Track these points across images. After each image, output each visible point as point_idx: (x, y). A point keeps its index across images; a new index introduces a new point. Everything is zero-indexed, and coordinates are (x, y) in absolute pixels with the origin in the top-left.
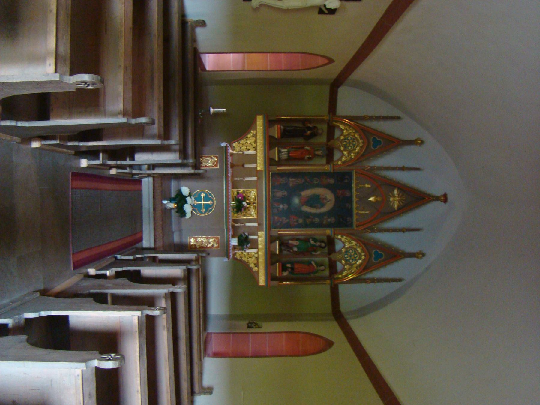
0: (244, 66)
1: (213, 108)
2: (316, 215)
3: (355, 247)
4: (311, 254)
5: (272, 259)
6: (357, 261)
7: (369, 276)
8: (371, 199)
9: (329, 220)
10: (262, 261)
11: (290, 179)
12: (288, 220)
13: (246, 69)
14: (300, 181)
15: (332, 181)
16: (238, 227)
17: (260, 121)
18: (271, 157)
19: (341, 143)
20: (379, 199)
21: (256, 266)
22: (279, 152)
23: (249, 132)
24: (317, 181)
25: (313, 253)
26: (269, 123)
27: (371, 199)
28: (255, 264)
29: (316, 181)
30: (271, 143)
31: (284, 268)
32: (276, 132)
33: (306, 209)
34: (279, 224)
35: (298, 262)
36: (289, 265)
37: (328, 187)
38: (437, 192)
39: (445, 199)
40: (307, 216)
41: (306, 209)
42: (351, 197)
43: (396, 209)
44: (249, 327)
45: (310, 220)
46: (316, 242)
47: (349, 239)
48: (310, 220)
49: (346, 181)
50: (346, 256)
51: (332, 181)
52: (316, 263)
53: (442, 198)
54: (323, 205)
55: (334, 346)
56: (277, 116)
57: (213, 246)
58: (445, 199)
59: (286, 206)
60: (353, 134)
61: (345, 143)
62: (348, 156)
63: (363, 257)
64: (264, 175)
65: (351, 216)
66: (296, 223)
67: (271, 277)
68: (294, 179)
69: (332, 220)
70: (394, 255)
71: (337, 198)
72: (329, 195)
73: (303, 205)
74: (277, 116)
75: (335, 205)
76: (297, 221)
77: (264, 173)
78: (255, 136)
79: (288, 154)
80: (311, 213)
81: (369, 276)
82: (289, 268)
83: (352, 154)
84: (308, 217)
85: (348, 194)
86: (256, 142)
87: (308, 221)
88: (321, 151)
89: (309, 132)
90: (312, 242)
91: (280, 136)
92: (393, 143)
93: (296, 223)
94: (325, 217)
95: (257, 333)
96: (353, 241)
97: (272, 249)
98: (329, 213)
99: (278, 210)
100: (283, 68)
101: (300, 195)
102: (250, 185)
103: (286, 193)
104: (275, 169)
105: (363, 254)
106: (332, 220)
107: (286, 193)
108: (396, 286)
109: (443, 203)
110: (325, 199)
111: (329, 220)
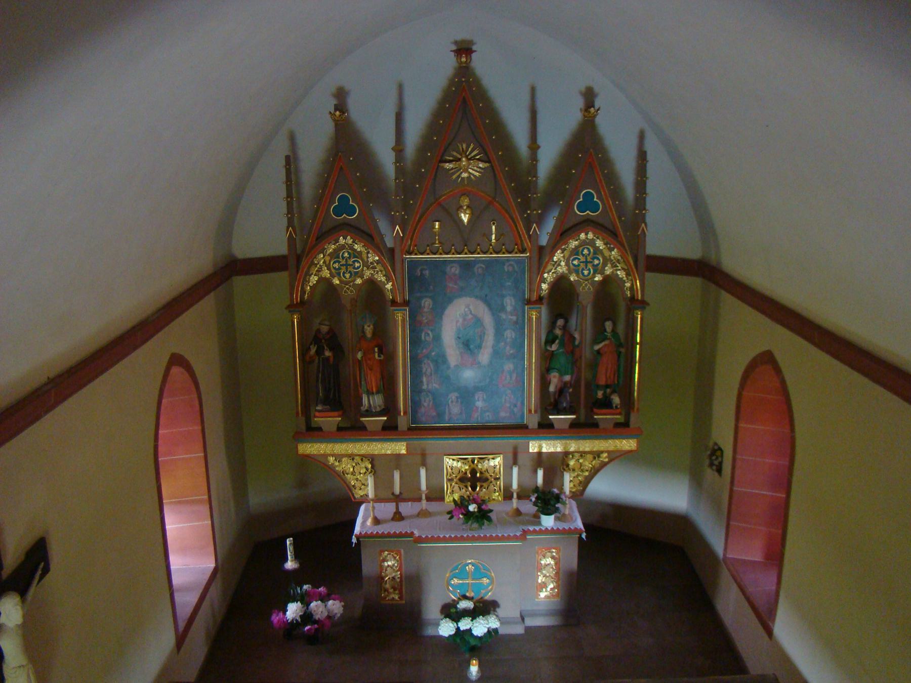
0: (200, 502)
1: (286, 560)
2: (499, 333)
3: (567, 253)
4: (578, 346)
5: (584, 427)
6: (597, 250)
7: (629, 192)
8: (465, 218)
10: (587, 445)
11: (425, 387)
12: (509, 392)
13: (206, 497)
16: (519, 485)
17: (310, 448)
18: (380, 428)
19: (347, 283)
20: (465, 201)
21: (599, 457)
22: (369, 413)
23: (331, 468)
25: (577, 343)
26: (313, 432)
27: (465, 218)
28: (594, 458)
29: (427, 336)
30: (353, 429)
31: (606, 404)
32: (329, 420)
33: (484, 357)
36: (600, 394)
37: (439, 310)
38: (449, 64)
39: (464, 50)
41: (484, 357)
43: (487, 165)
44: (719, 470)
46: (556, 338)
47: (549, 267)
48: (508, 348)
50: (586, 272)
52: (595, 341)
53: (464, 60)
54: (478, 321)
56: (297, 414)
57: (553, 557)
58: (464, 50)
60: (327, 258)
61: (348, 276)
62: (374, 268)
63: (590, 236)
67: (622, 428)
68: (424, 379)
70: (586, 147)
74: (297, 414)
78: (339, 457)
79: (373, 393)
81: (629, 192)
82: (604, 394)
83: (370, 260)
86: (352, 457)
87: (509, 351)
88: (366, 327)
89: (328, 353)
90: (554, 347)
91: (336, 414)
92: (347, 144)
94: (503, 316)
95: (734, 460)
96: (555, 259)
97: (566, 426)
98: (496, 310)
100: (198, 428)
101: (456, 366)
102: (436, 470)
104: (403, 422)
105: (583, 236)
108: (652, 146)
109: (474, 55)
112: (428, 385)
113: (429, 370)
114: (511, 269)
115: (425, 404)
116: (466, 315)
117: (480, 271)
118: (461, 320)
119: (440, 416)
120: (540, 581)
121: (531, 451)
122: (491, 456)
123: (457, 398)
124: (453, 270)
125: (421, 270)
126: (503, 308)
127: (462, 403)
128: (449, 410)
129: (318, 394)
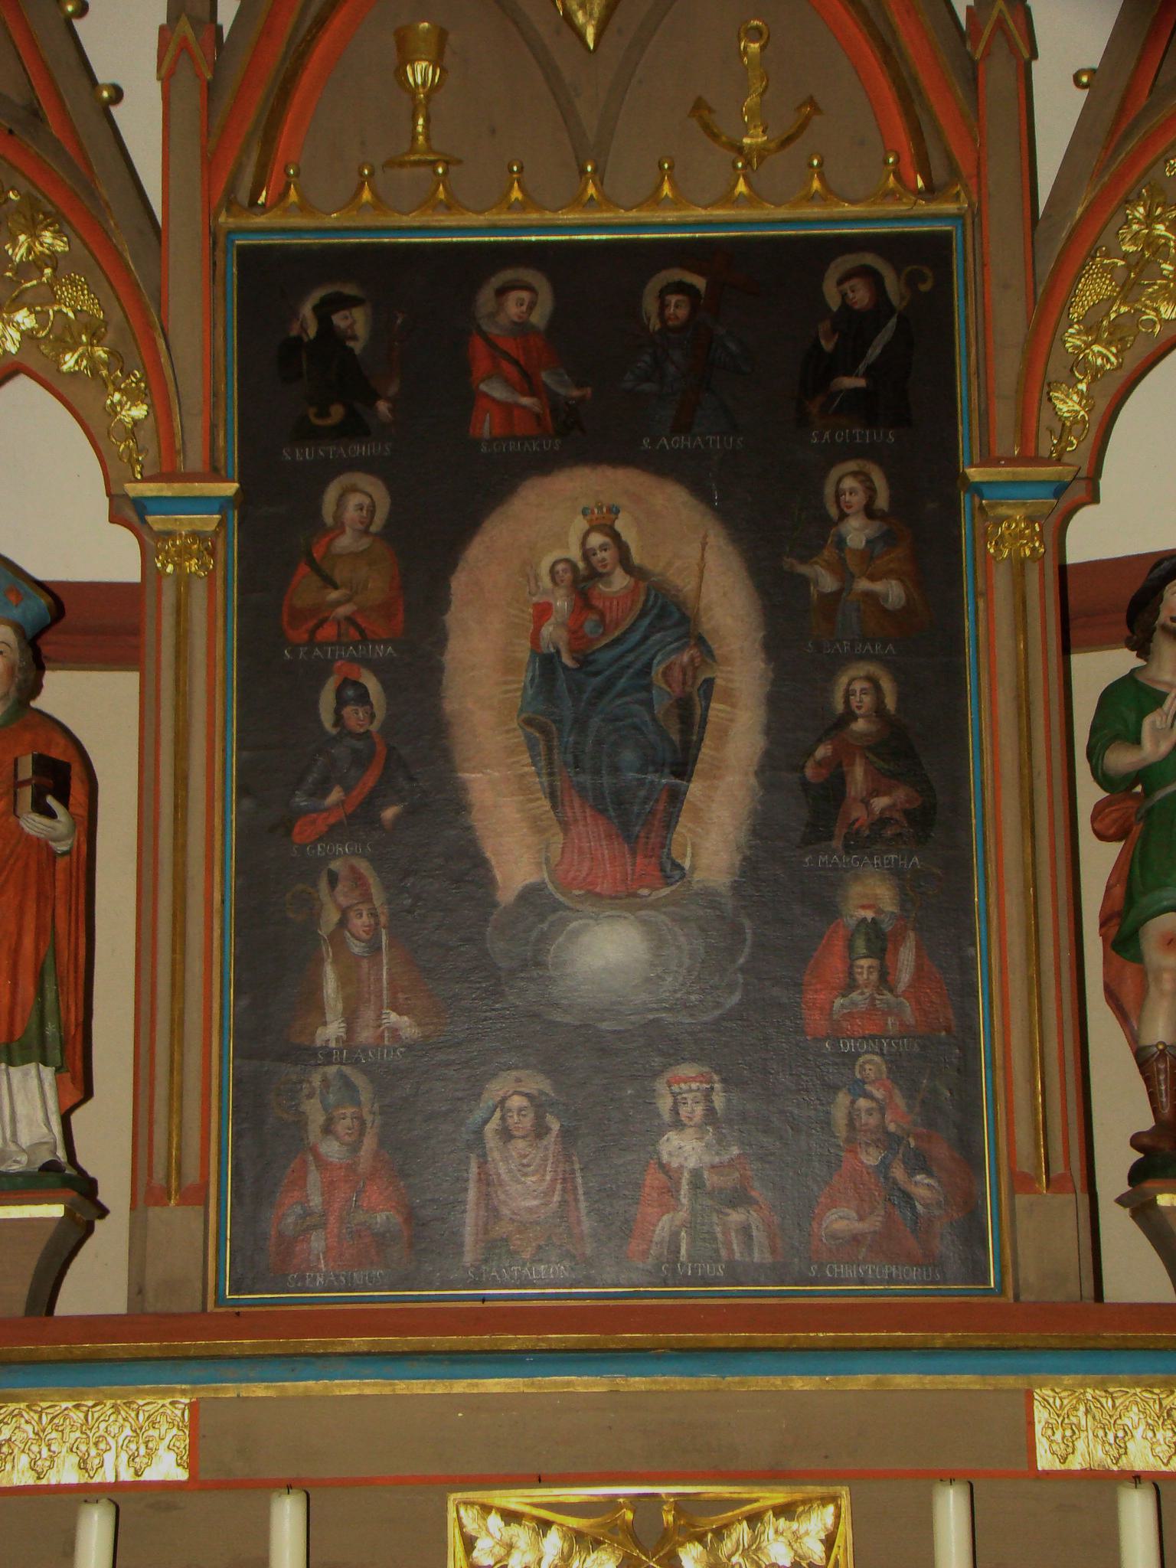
9: (856, 532)
11: (332, 1031)
12: (871, 1065)
14: (350, 905)
15: (355, 503)
24: (352, 693)
33: (715, 827)
34: (923, 1187)
35: (889, 195)
37: (429, 543)
40: (804, 811)
41: (715, 827)
42: (561, 262)
45: (858, 775)
49: (356, 324)
51: (355, 503)
54: (670, 614)
55: (108, 1217)
59: (685, 1088)
64: (230, 1391)
65: (807, 256)
66: (906, 958)
69: (855, 496)
71: (576, 437)
72: (544, 529)
73: (671, 871)
75: (661, 465)
76: (879, 940)
77: (206, 1391)
80: (778, 763)
84: (827, 798)
85: (523, 305)
93: (906, 958)
98: (773, 528)
99: (739, 1198)
101: (531, 895)
103: (513, 1091)
106: (855, 496)
107: (513, 1091)
110: (583, 582)
111: (856, 532)
112: (351, 1018)
113: (360, 922)
114: (860, 295)
115: (332, 1150)
116: (595, 575)
117: (678, 308)
118: (561, 603)
119: (423, 1235)
120: (1164, 266)
121: (1045, 1461)
122: (777, 1496)
123: (539, 1105)
124: (514, 306)
125: (325, 310)
126: (821, 528)
127: (568, 1135)
128: (486, 1181)
129: (426, 126)
